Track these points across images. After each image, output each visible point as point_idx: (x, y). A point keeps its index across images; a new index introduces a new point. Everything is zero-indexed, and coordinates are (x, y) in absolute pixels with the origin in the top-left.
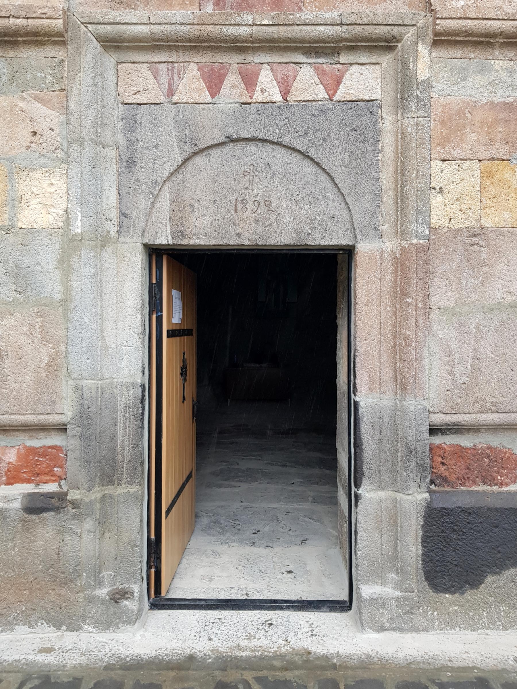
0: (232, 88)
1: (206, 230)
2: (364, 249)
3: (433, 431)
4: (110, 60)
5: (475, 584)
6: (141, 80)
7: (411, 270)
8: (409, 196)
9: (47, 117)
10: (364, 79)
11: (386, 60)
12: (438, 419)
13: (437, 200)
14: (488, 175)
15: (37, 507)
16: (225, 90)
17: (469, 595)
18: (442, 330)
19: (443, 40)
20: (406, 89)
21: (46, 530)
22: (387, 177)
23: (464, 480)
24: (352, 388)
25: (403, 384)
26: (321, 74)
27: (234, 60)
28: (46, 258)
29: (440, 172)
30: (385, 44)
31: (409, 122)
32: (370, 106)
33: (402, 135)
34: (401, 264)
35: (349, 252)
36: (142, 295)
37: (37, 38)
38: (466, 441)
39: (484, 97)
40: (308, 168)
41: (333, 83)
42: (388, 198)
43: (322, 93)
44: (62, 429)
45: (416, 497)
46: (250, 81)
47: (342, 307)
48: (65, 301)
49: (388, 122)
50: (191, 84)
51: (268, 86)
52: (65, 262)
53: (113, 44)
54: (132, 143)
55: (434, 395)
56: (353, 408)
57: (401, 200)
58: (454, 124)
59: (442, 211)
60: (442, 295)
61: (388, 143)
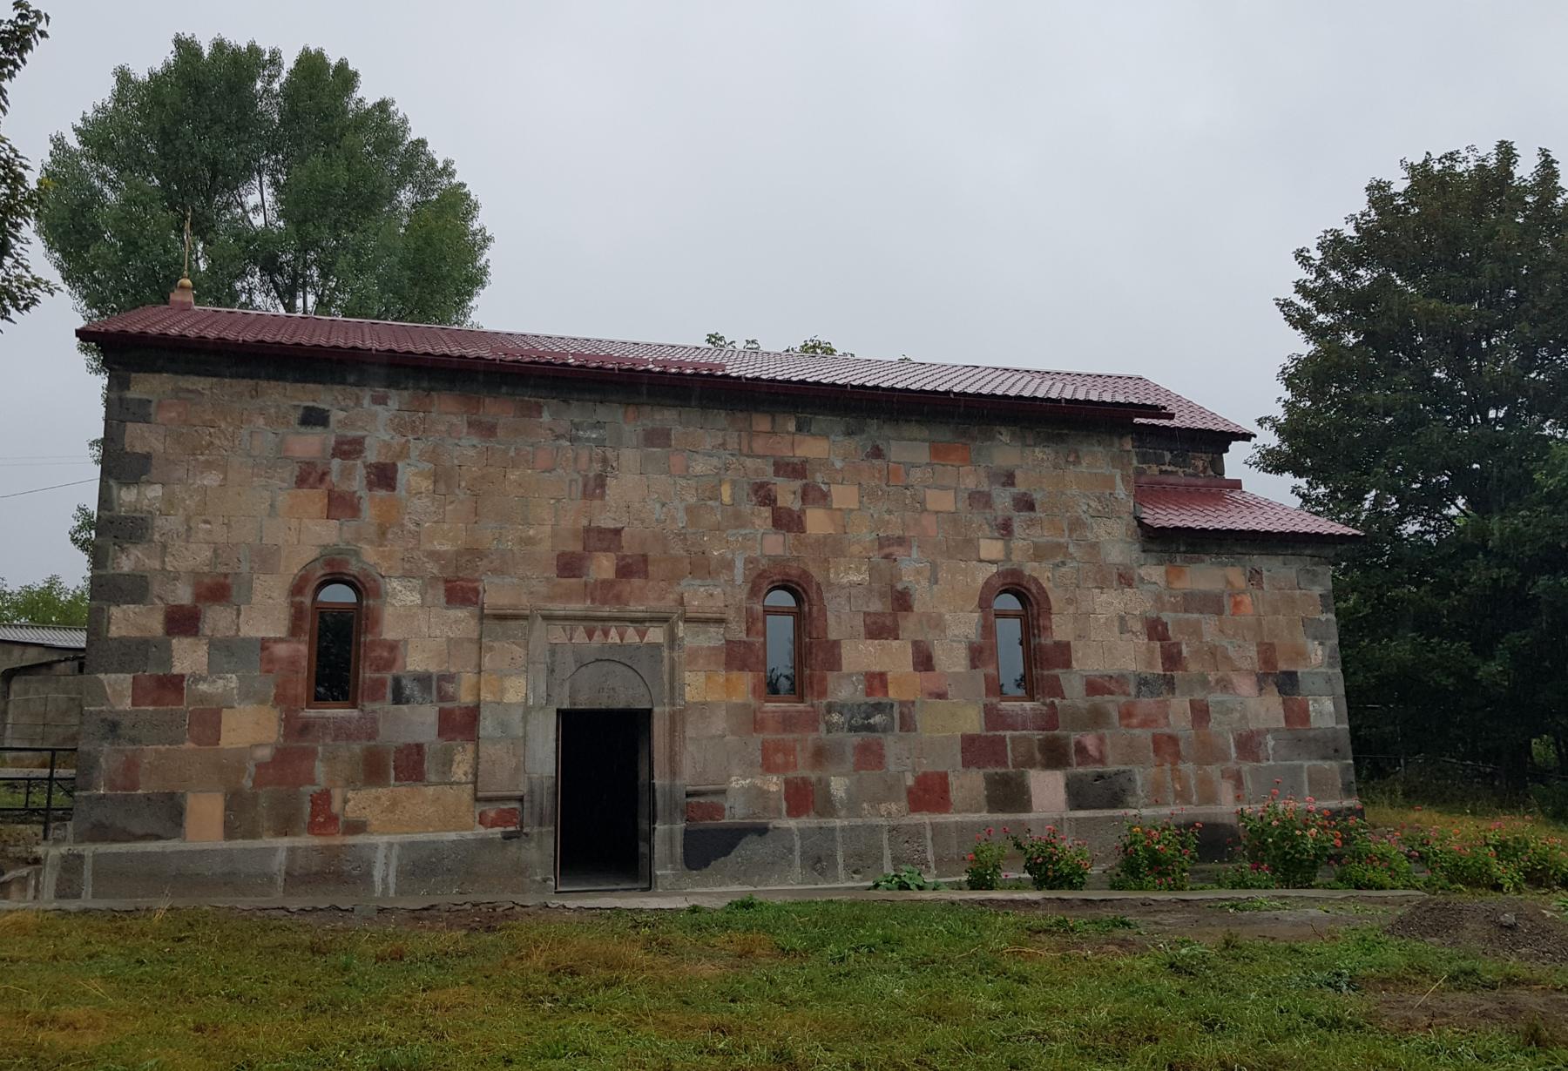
0: (598, 637)
1: (585, 701)
2: (656, 710)
3: (688, 795)
4: (544, 624)
5: (707, 865)
6: (558, 634)
7: (675, 720)
8: (674, 688)
9: (518, 651)
10: (656, 634)
11: (665, 625)
12: (689, 788)
13: (687, 689)
14: (708, 678)
15: (508, 837)
16: (595, 638)
17: (705, 871)
18: (691, 748)
19: (687, 620)
20: (672, 639)
21: (513, 848)
22: (666, 677)
23: (702, 818)
24: (651, 777)
25: (674, 773)
26: (638, 631)
27: (599, 625)
28: (517, 716)
29: (688, 677)
30: (666, 620)
31: (675, 655)
32: (658, 646)
33: (672, 659)
34: (672, 717)
35: (650, 711)
36: (1214, 416)
37: (525, 618)
38: (702, 800)
39: (706, 645)
40: (631, 673)
41: (642, 635)
42: (667, 687)
43: (637, 639)
44: (521, 799)
45: (680, 826)
46: (606, 633)
47: (643, 755)
48: (525, 736)
49: (666, 653)
50: (580, 636)
51: (614, 637)
52: (525, 719)
53: (548, 618)
54: (553, 662)
55: (687, 778)
56: (652, 787)
57: (672, 688)
58: (694, 655)
59: (691, 694)
60: (690, 732)
61: (666, 661)
